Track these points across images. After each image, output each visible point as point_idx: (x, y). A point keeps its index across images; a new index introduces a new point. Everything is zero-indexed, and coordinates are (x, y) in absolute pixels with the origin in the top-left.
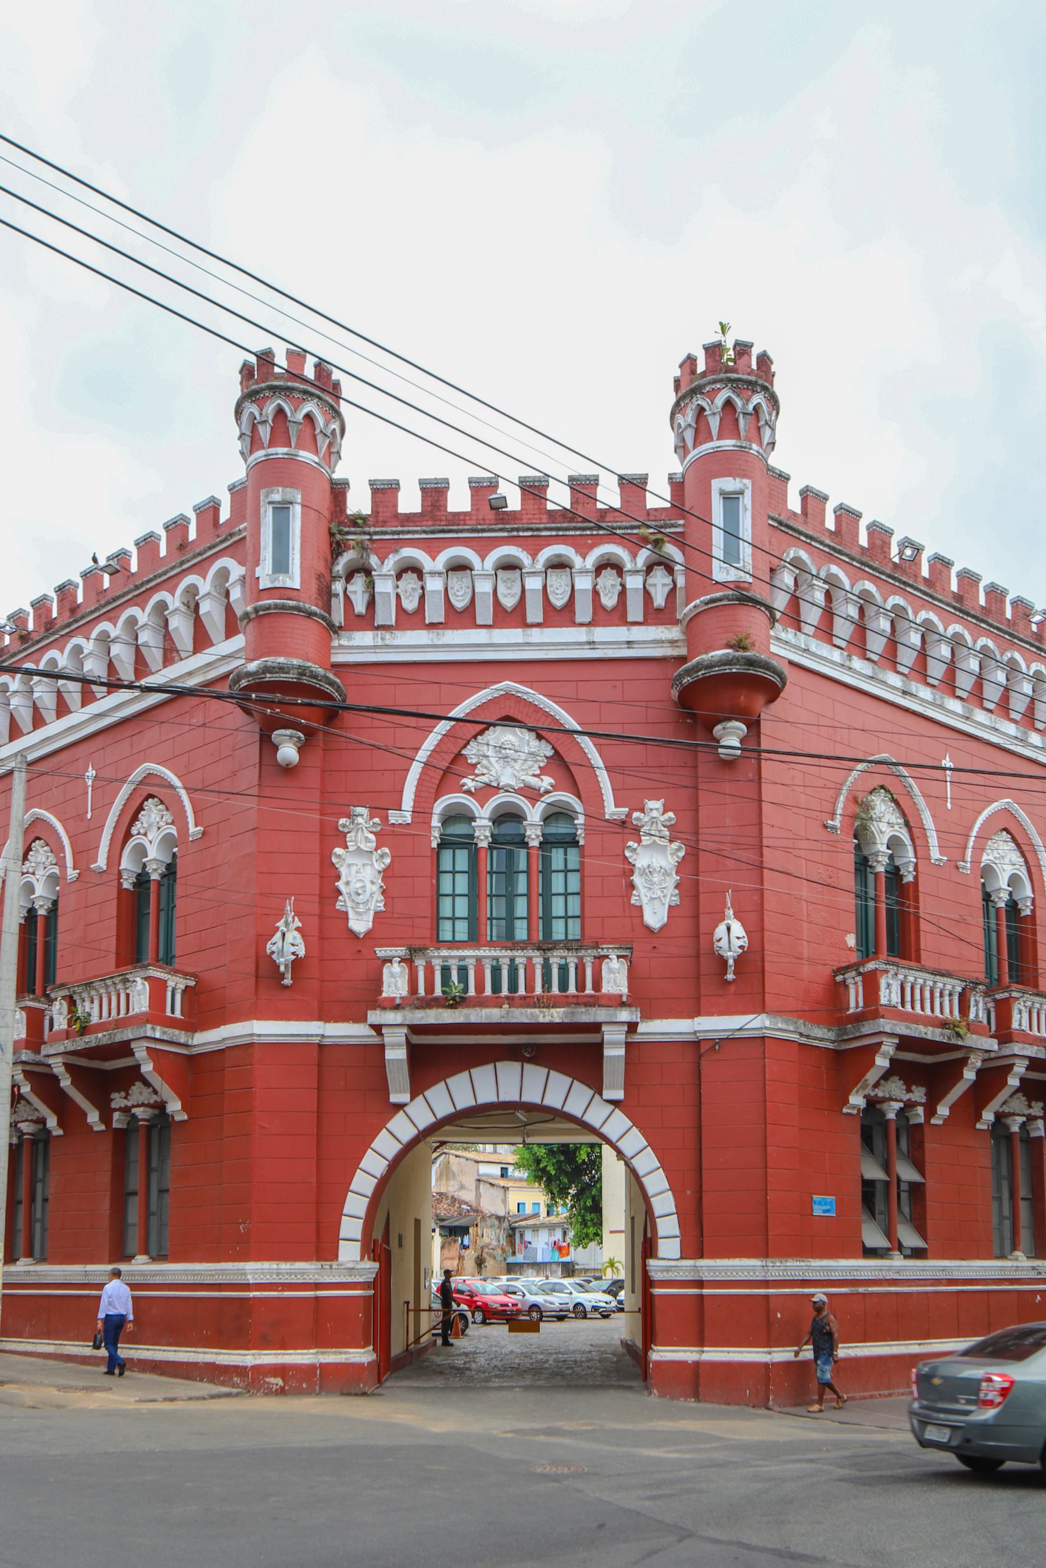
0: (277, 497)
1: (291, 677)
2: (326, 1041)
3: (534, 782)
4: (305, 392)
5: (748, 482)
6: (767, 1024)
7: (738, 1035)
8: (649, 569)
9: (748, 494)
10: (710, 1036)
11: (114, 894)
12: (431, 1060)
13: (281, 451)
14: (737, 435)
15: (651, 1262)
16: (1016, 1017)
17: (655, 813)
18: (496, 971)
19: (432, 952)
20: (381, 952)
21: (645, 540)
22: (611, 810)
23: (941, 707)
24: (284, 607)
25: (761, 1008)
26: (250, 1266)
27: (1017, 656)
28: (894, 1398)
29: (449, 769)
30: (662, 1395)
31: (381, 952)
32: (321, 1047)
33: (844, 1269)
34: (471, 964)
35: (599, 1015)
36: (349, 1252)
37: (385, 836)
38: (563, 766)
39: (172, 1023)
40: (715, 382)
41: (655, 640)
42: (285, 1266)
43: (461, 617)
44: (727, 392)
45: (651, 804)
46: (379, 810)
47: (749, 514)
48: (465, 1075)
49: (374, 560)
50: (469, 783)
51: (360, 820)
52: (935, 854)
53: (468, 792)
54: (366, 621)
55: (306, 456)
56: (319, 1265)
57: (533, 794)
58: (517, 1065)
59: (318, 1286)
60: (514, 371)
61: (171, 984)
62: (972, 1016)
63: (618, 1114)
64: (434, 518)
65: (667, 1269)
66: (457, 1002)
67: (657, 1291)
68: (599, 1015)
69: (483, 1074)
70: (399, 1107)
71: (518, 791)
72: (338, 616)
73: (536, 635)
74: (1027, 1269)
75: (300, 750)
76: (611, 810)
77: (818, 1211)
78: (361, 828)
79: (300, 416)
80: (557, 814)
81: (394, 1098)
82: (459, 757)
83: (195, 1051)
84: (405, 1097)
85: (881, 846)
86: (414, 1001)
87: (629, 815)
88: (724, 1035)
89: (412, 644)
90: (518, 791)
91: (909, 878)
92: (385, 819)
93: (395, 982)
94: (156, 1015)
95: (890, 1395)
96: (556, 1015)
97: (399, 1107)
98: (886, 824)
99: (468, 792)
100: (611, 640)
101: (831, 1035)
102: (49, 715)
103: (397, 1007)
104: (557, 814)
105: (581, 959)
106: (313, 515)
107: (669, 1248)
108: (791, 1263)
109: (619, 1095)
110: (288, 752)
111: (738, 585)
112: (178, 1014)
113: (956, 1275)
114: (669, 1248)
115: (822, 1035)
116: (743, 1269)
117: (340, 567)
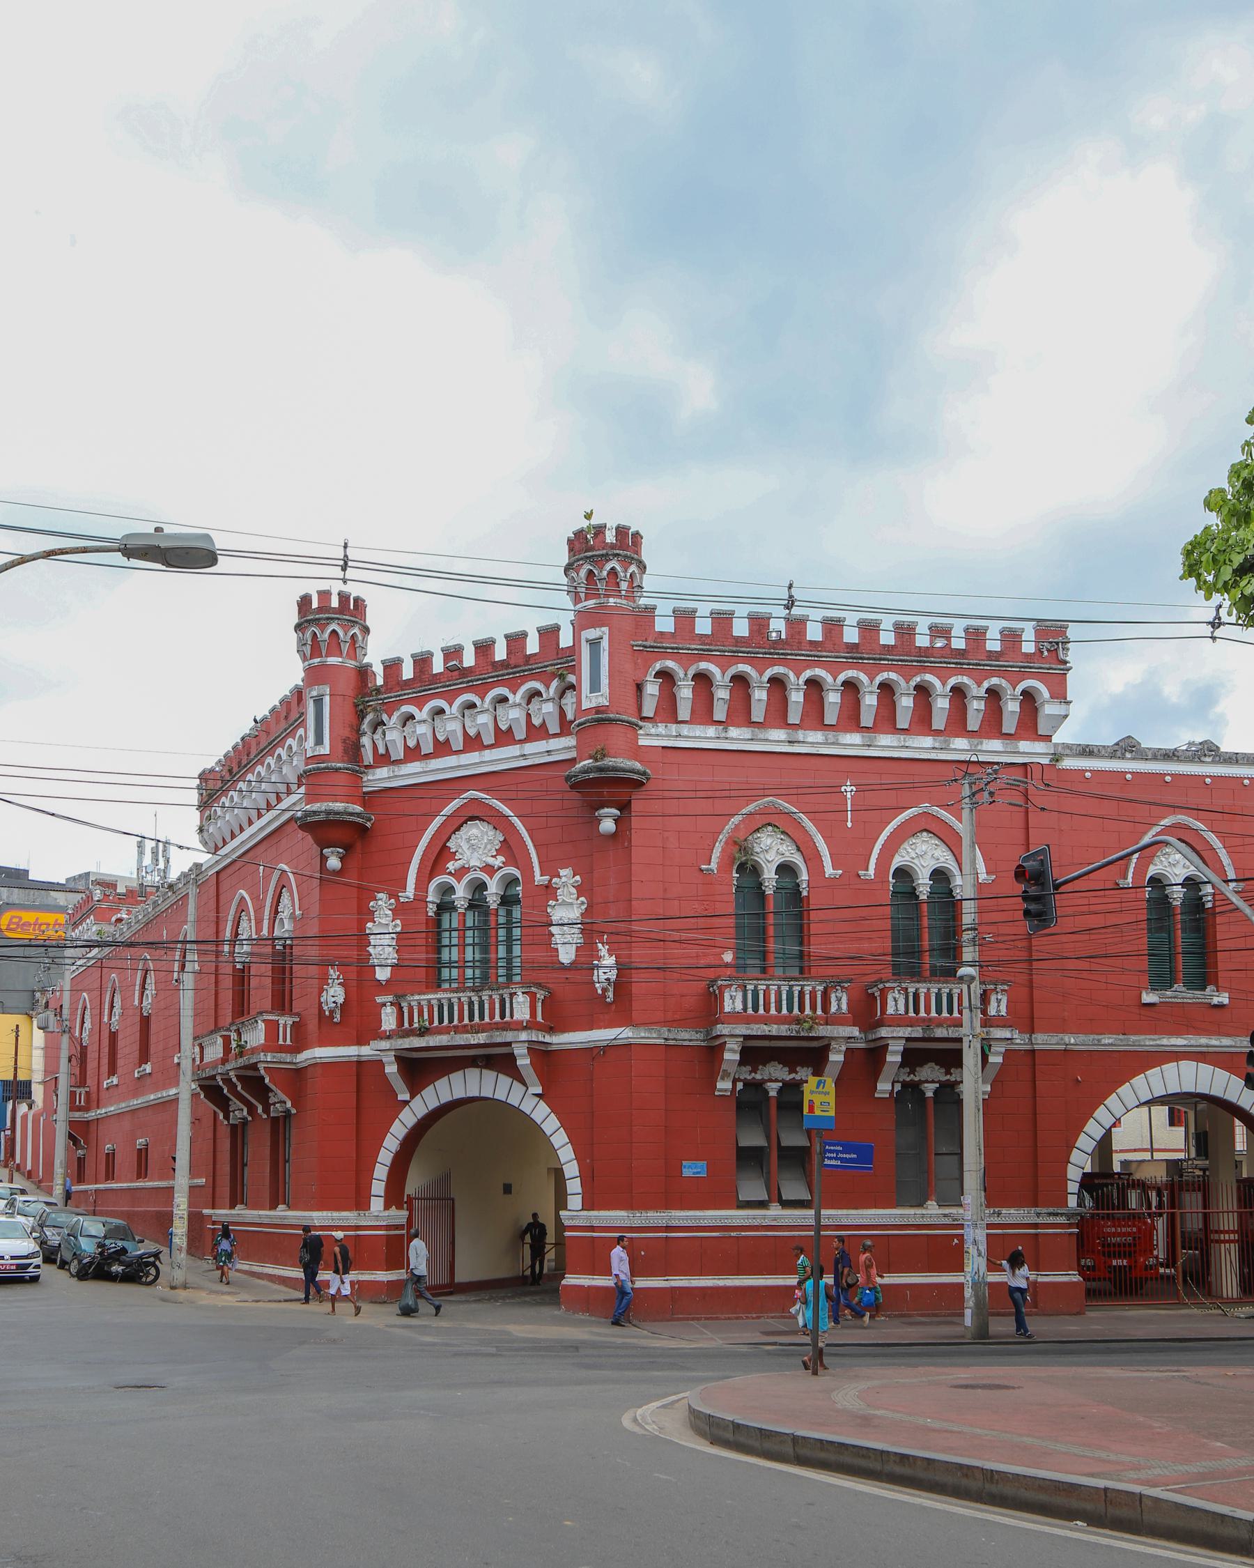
0: (314, 693)
1: (322, 817)
2: (363, 1059)
3: (491, 861)
4: (328, 619)
5: (606, 629)
6: (630, 1035)
7: (615, 1042)
8: (562, 695)
9: (606, 638)
10: (599, 1044)
11: (138, 1019)
12: (419, 1069)
13: (317, 660)
14: (598, 596)
15: (561, 1213)
16: (890, 1002)
17: (567, 878)
18: (441, 1007)
19: (409, 998)
20: (379, 1000)
21: (553, 675)
22: (539, 879)
23: (836, 743)
24: (318, 769)
25: (627, 1021)
26: (315, 1214)
27: (928, 677)
28: (762, 1320)
29: (440, 856)
30: (568, 1310)
31: (379, 1000)
32: (359, 1063)
33: (712, 1218)
34: (434, 1002)
35: (508, 1036)
36: (377, 1204)
37: (400, 910)
38: (510, 848)
39: (282, 1049)
40: (578, 560)
41: (561, 747)
42: (336, 1214)
43: (442, 748)
44: (602, 557)
45: (562, 872)
46: (393, 895)
47: (606, 653)
48: (461, 1072)
49: (385, 717)
50: (451, 866)
51: (380, 903)
52: (829, 870)
53: (450, 873)
54: (384, 759)
55: (332, 660)
56: (355, 1213)
57: (490, 870)
58: (477, 1071)
59: (358, 1228)
60: (460, 571)
61: (282, 1022)
62: (833, 1009)
63: (542, 1104)
64: (421, 681)
65: (572, 1218)
66: (423, 1032)
67: (567, 1234)
68: (508, 1036)
69: (456, 1077)
70: (406, 1103)
71: (482, 869)
72: (368, 757)
73: (488, 755)
74: (937, 1216)
75: (342, 859)
76: (539, 879)
77: (687, 1172)
78: (382, 904)
79: (326, 635)
80: (511, 882)
81: (400, 1098)
82: (444, 848)
83: (300, 1066)
84: (406, 1097)
85: (769, 875)
86: (401, 1032)
87: (550, 881)
88: (605, 1043)
89: (413, 773)
90: (482, 869)
91: (805, 893)
92: (397, 899)
93: (388, 1020)
94: (272, 1044)
95: (758, 1318)
96: (481, 1038)
97: (406, 1103)
98: (772, 851)
99: (450, 873)
100: (537, 751)
101: (700, 1036)
102: (245, 825)
103: (389, 1037)
104: (511, 882)
105: (501, 995)
106: (339, 699)
107: (575, 1202)
108: (650, 1214)
109: (539, 1090)
110: (334, 863)
111: (598, 710)
112: (288, 1042)
113: (845, 1222)
114: (575, 1202)
115: (688, 1036)
116: (617, 1218)
117: (365, 726)
